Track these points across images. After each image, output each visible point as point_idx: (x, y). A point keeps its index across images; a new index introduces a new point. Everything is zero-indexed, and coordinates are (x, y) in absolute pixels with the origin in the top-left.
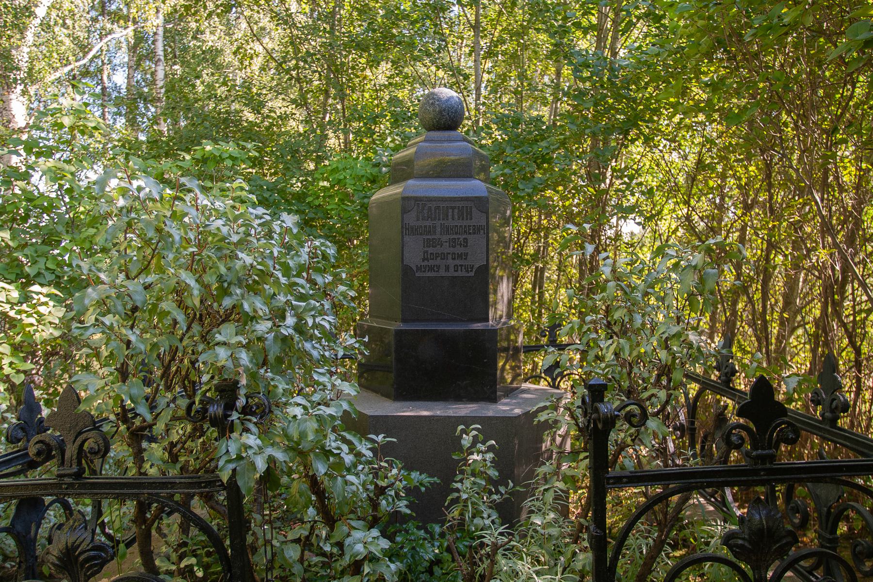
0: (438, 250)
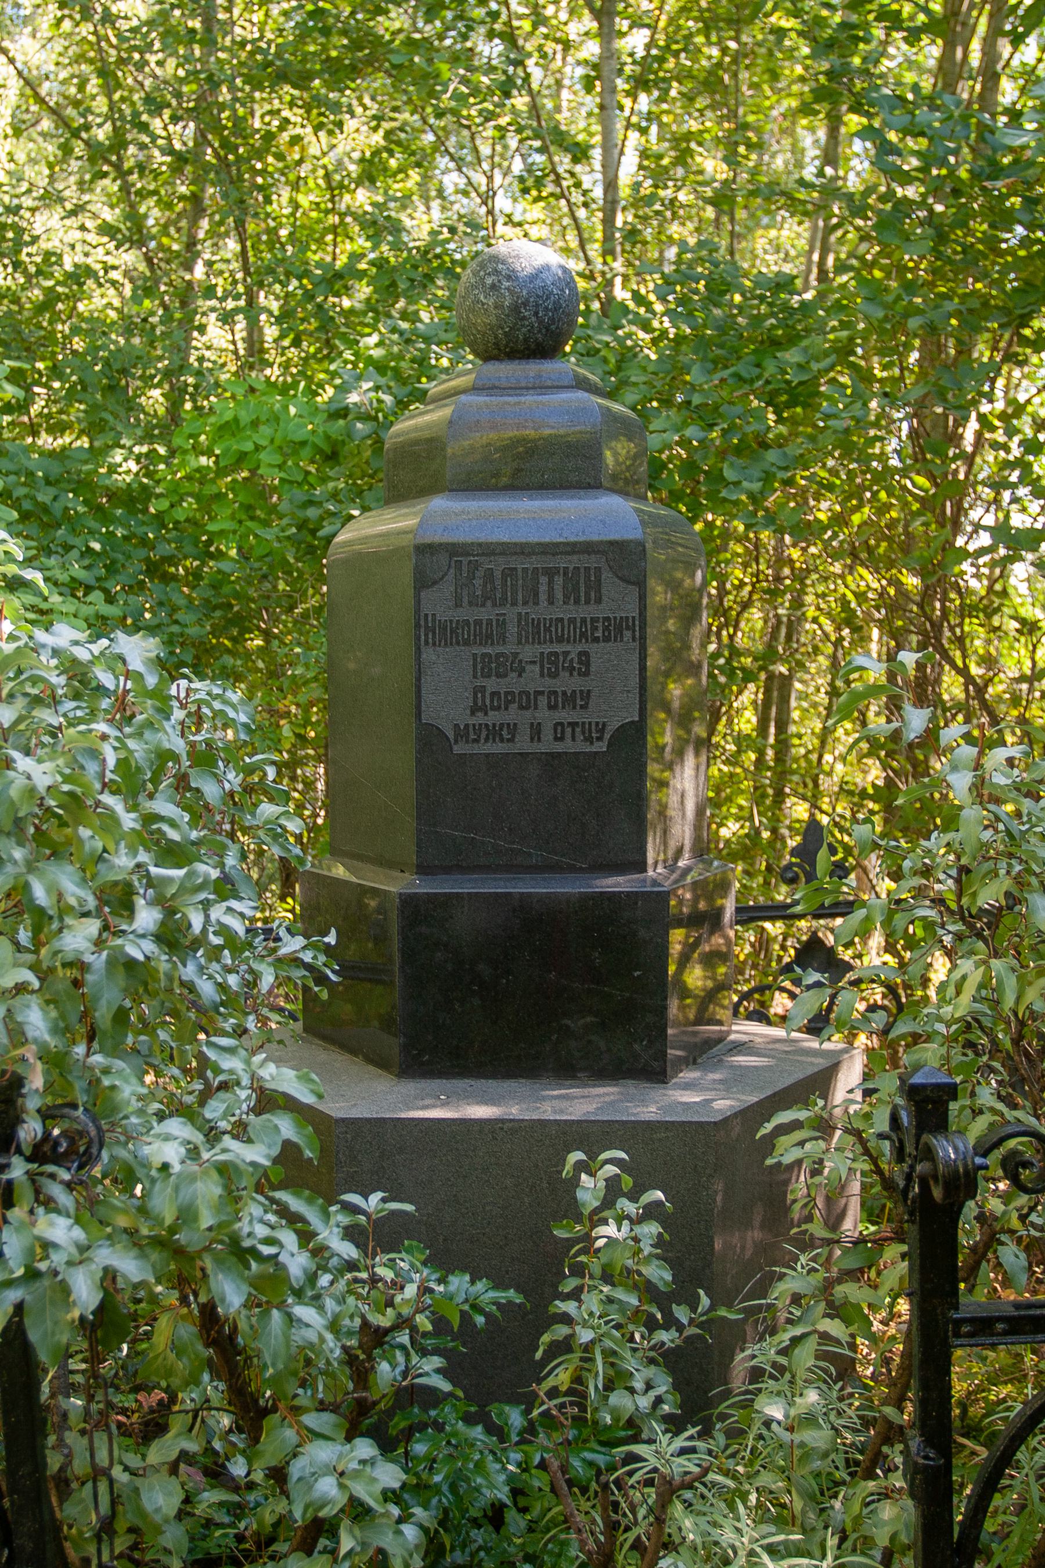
0: (511, 683)
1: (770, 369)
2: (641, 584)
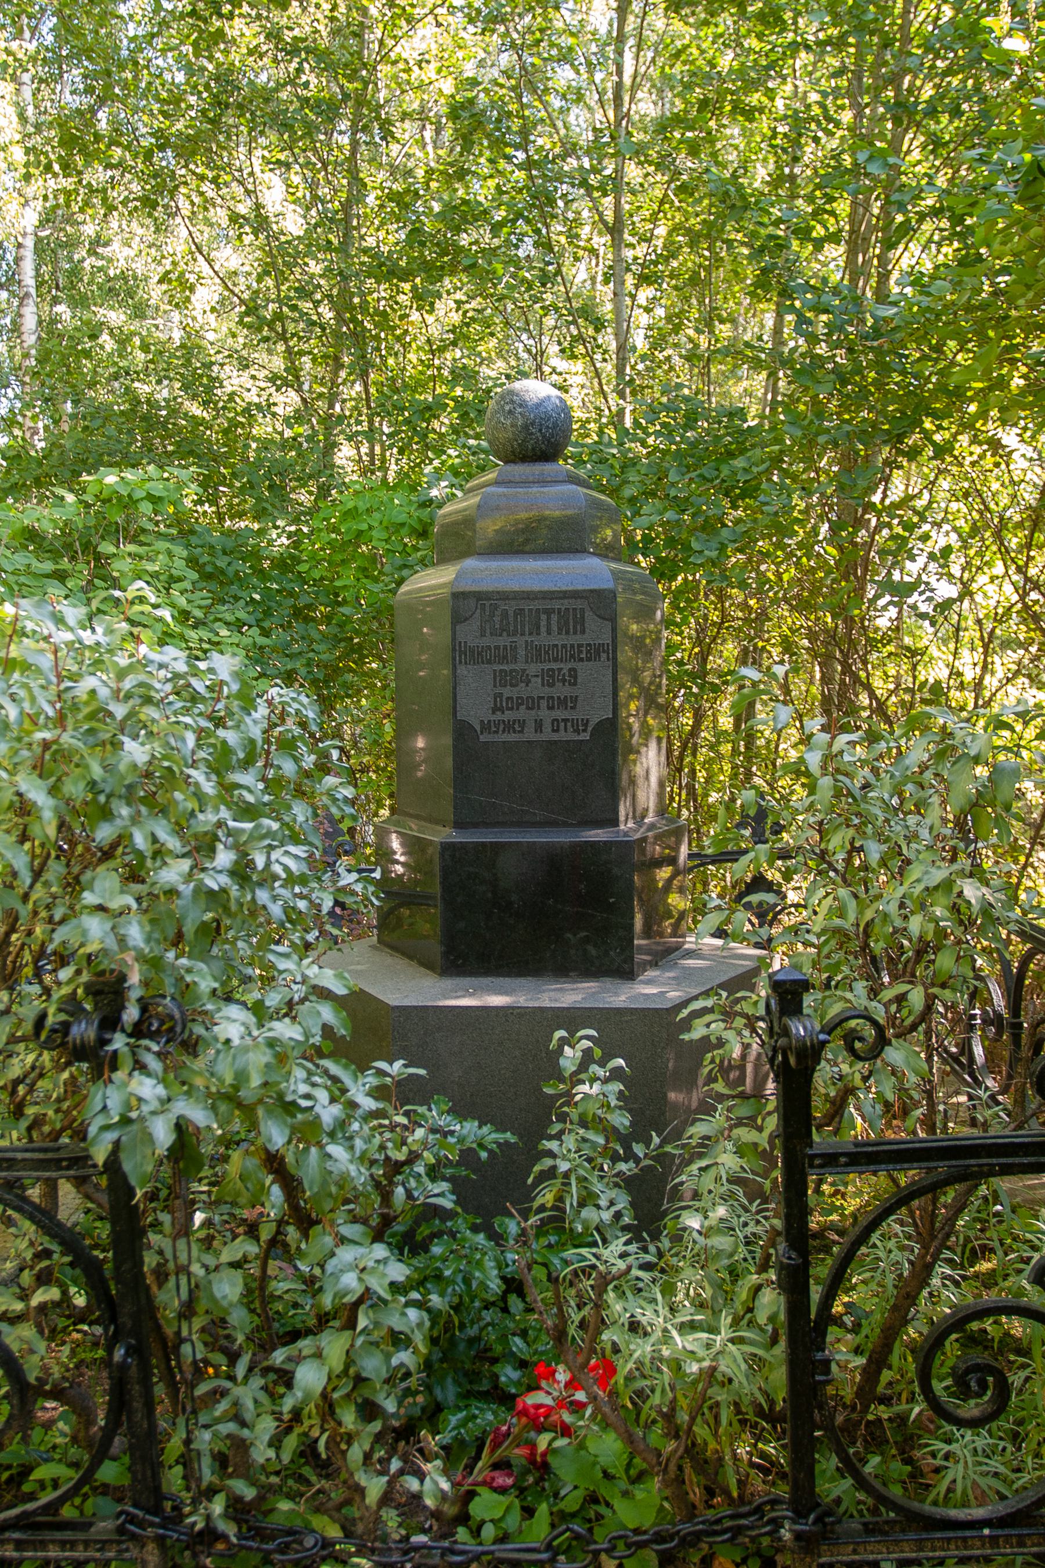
0: (521, 691)
1: (725, 472)
2: (613, 620)
